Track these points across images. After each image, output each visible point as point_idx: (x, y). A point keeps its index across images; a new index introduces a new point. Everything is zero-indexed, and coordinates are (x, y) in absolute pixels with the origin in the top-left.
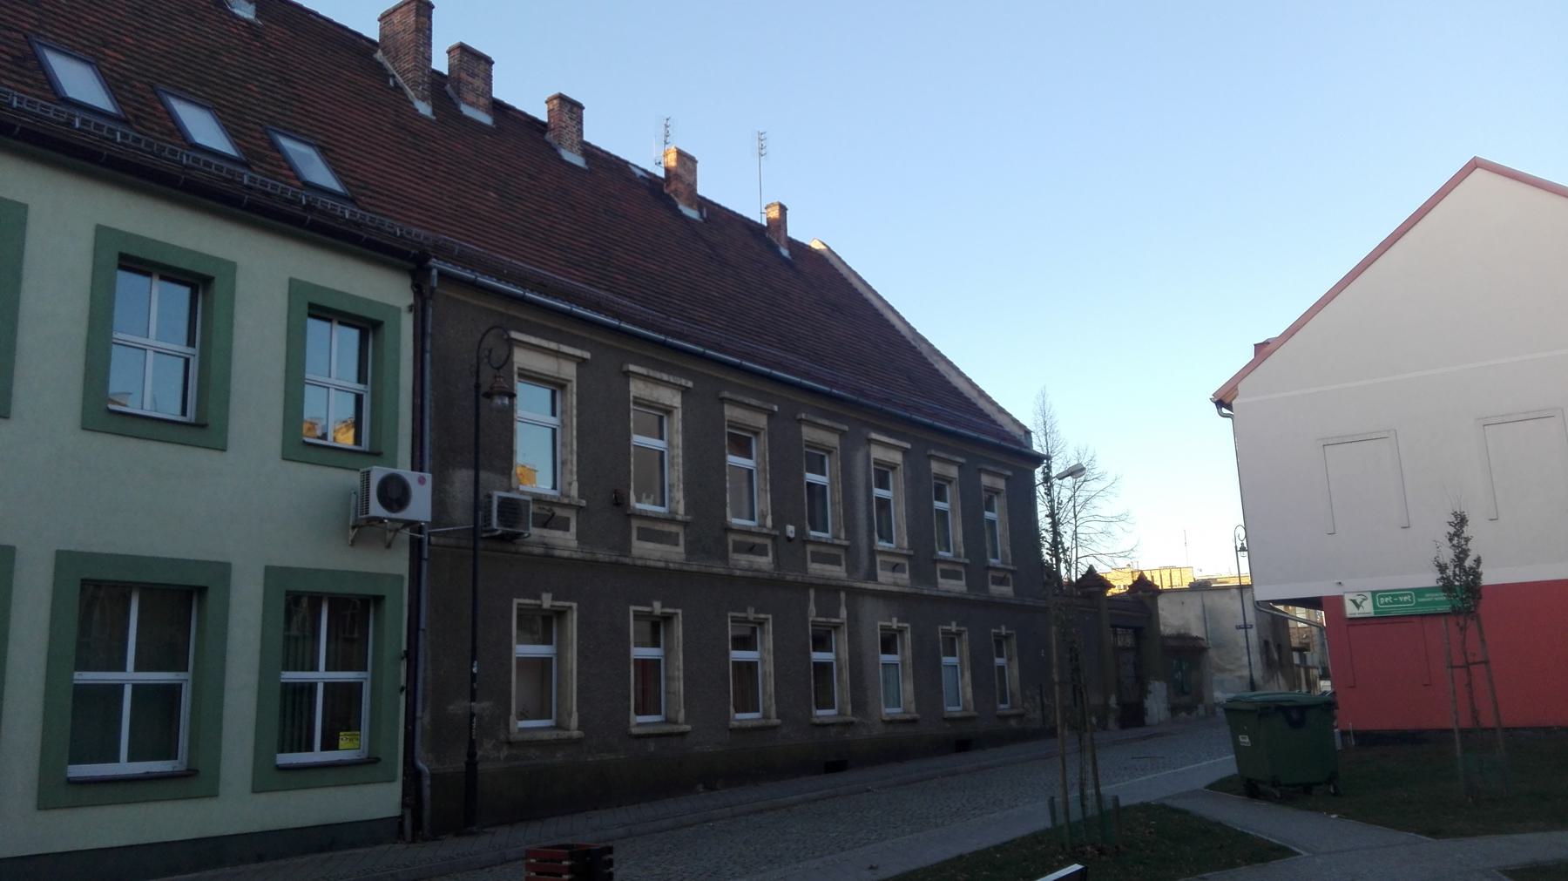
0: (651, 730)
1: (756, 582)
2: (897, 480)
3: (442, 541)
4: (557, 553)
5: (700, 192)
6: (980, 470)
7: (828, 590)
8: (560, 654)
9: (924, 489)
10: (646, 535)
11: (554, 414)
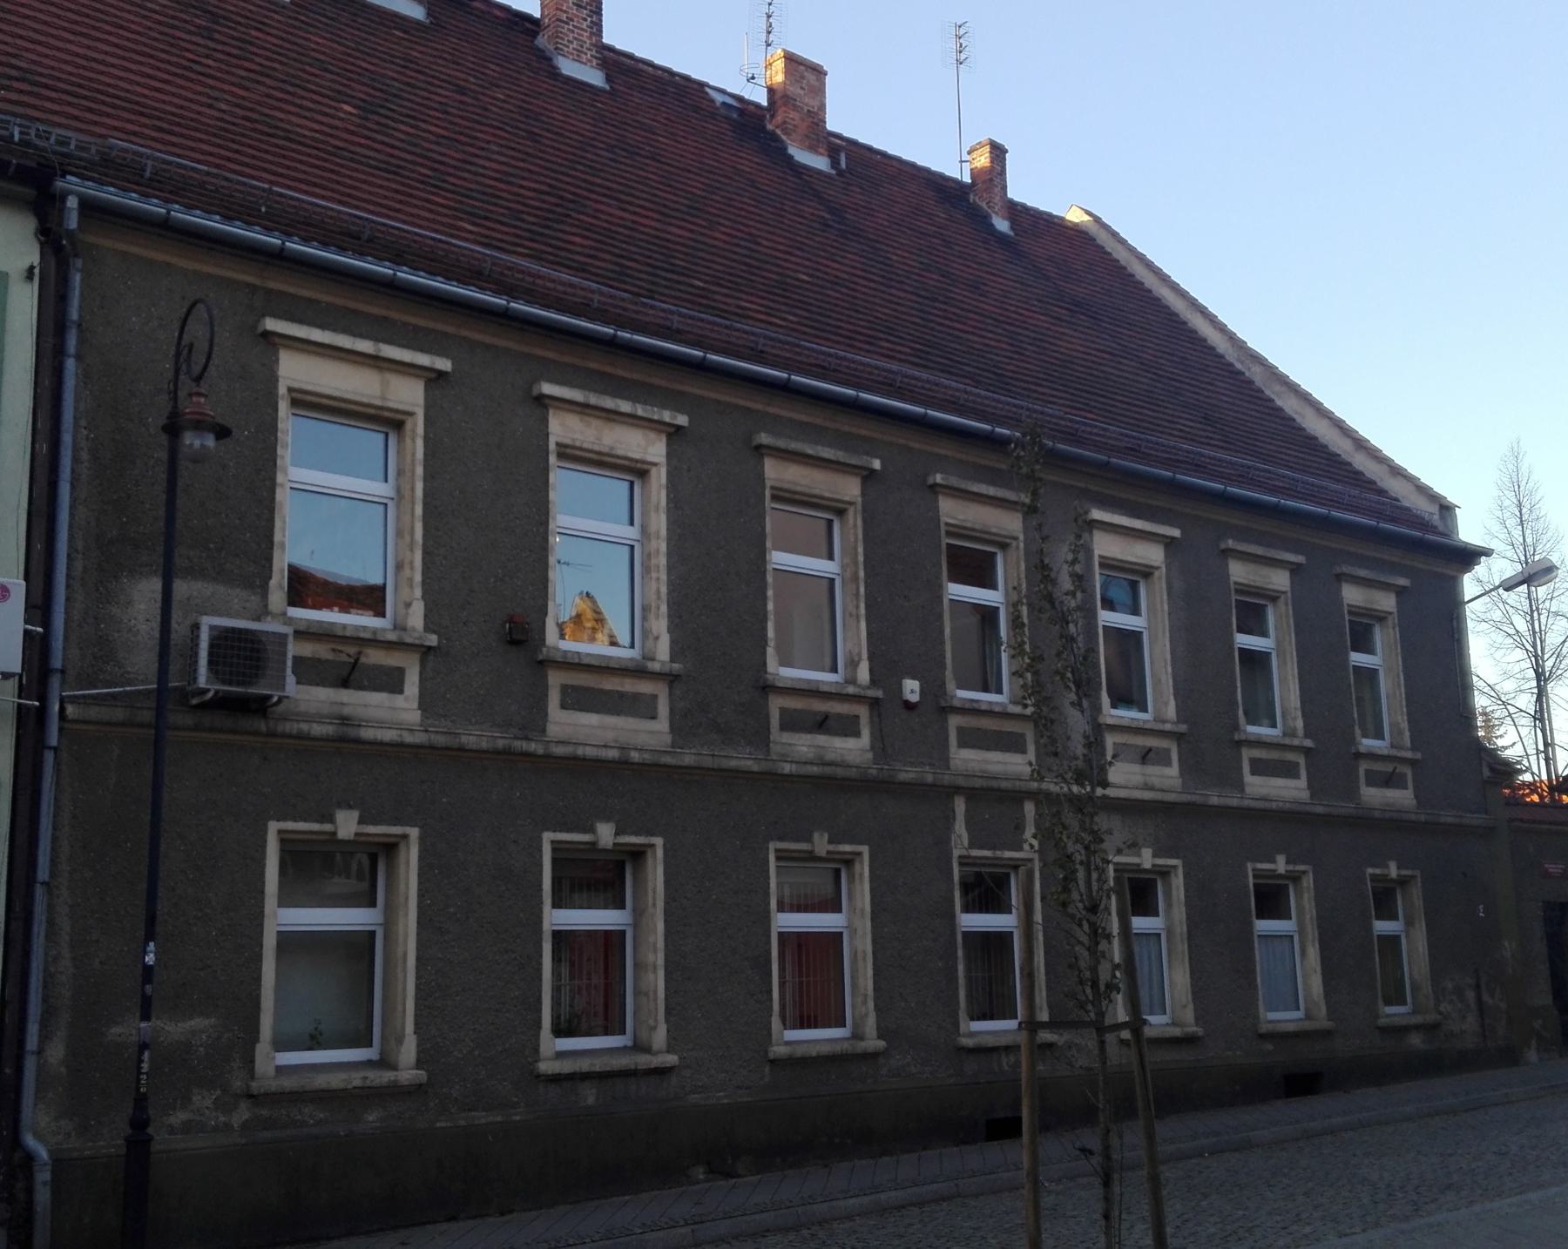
0: (598, 1065)
1: (831, 787)
2: (1154, 596)
3: (93, 713)
4: (367, 734)
5: (832, 125)
6: (1340, 578)
7: (994, 799)
8: (389, 923)
9: (1209, 613)
10: (577, 699)
11: (632, 524)
